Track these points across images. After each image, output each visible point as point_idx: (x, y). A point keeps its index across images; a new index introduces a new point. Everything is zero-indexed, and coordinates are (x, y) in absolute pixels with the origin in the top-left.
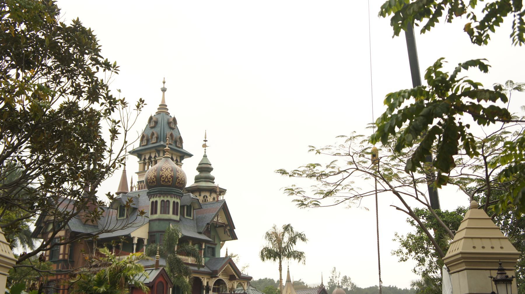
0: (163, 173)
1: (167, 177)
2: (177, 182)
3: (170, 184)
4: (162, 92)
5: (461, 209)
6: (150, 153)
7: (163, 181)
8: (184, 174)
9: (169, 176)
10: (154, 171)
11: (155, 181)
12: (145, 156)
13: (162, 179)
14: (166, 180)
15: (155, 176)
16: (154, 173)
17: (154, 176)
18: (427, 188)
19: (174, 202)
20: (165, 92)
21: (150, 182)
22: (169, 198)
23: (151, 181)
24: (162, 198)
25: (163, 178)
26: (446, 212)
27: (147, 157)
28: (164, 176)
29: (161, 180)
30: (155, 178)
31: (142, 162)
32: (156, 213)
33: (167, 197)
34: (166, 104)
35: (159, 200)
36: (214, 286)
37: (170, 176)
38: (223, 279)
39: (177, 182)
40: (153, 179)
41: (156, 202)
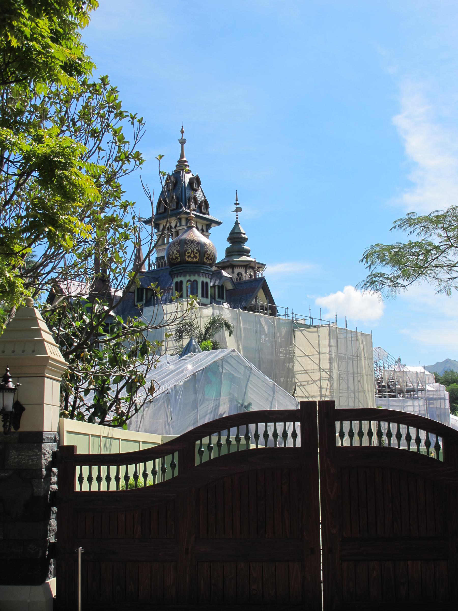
2: (186, 257)
3: (197, 260)
7: (207, 258)
10: (188, 250)
14: (174, 257)
25: (188, 253)
33: (194, 276)
37: (197, 250)
40: (176, 254)
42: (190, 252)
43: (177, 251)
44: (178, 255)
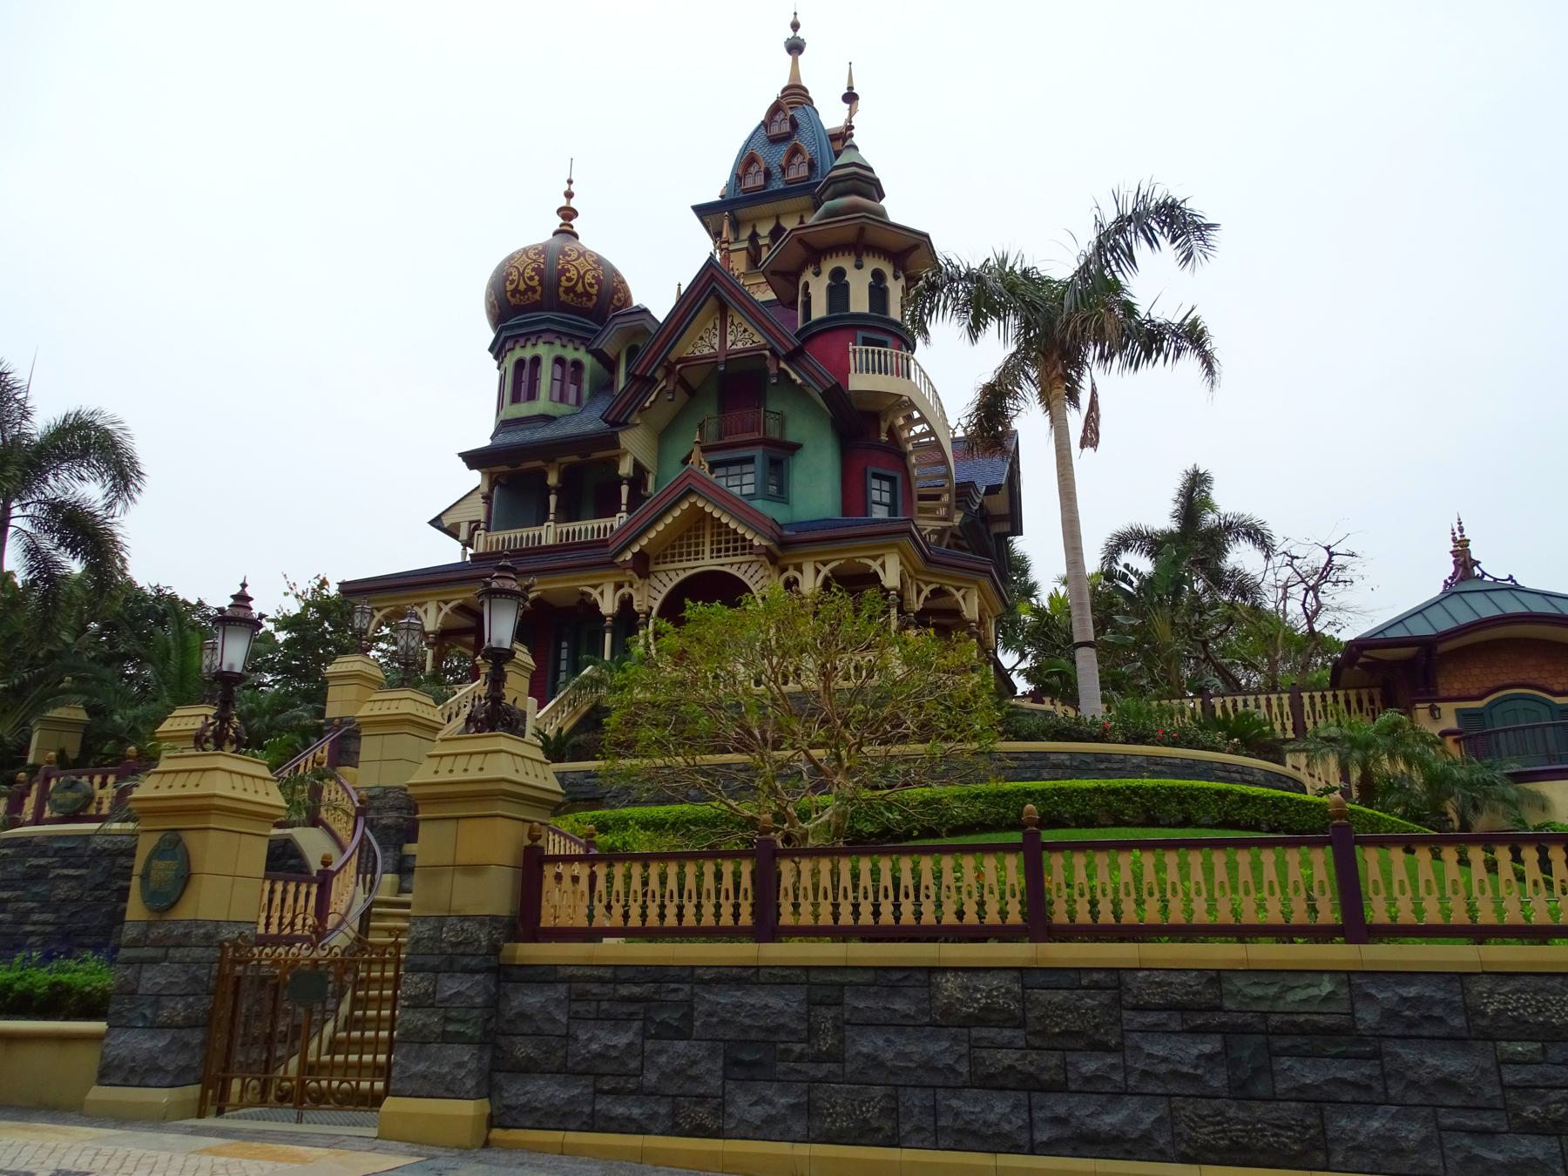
0: (568, 262)
1: (581, 277)
4: (790, 58)
5: (114, 445)
6: (778, 218)
7: (568, 290)
8: (599, 261)
9: (589, 278)
11: (539, 289)
12: (754, 227)
13: (564, 283)
14: (580, 288)
15: (537, 270)
16: (535, 261)
17: (533, 269)
18: (687, 276)
19: (559, 361)
20: (801, 58)
21: (515, 291)
22: (542, 350)
23: (580, 288)
24: (558, 350)
25: (569, 279)
26: (1017, 559)
27: (764, 230)
28: (573, 274)
29: (559, 285)
30: (537, 278)
31: (745, 245)
32: (532, 396)
33: (534, 345)
34: (804, 83)
35: (546, 352)
36: (125, 884)
38: (733, 571)
39: (561, 289)
40: (531, 278)
41: (536, 361)
42: (575, 277)
43: (593, 277)
44: (535, 283)
